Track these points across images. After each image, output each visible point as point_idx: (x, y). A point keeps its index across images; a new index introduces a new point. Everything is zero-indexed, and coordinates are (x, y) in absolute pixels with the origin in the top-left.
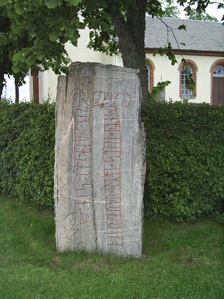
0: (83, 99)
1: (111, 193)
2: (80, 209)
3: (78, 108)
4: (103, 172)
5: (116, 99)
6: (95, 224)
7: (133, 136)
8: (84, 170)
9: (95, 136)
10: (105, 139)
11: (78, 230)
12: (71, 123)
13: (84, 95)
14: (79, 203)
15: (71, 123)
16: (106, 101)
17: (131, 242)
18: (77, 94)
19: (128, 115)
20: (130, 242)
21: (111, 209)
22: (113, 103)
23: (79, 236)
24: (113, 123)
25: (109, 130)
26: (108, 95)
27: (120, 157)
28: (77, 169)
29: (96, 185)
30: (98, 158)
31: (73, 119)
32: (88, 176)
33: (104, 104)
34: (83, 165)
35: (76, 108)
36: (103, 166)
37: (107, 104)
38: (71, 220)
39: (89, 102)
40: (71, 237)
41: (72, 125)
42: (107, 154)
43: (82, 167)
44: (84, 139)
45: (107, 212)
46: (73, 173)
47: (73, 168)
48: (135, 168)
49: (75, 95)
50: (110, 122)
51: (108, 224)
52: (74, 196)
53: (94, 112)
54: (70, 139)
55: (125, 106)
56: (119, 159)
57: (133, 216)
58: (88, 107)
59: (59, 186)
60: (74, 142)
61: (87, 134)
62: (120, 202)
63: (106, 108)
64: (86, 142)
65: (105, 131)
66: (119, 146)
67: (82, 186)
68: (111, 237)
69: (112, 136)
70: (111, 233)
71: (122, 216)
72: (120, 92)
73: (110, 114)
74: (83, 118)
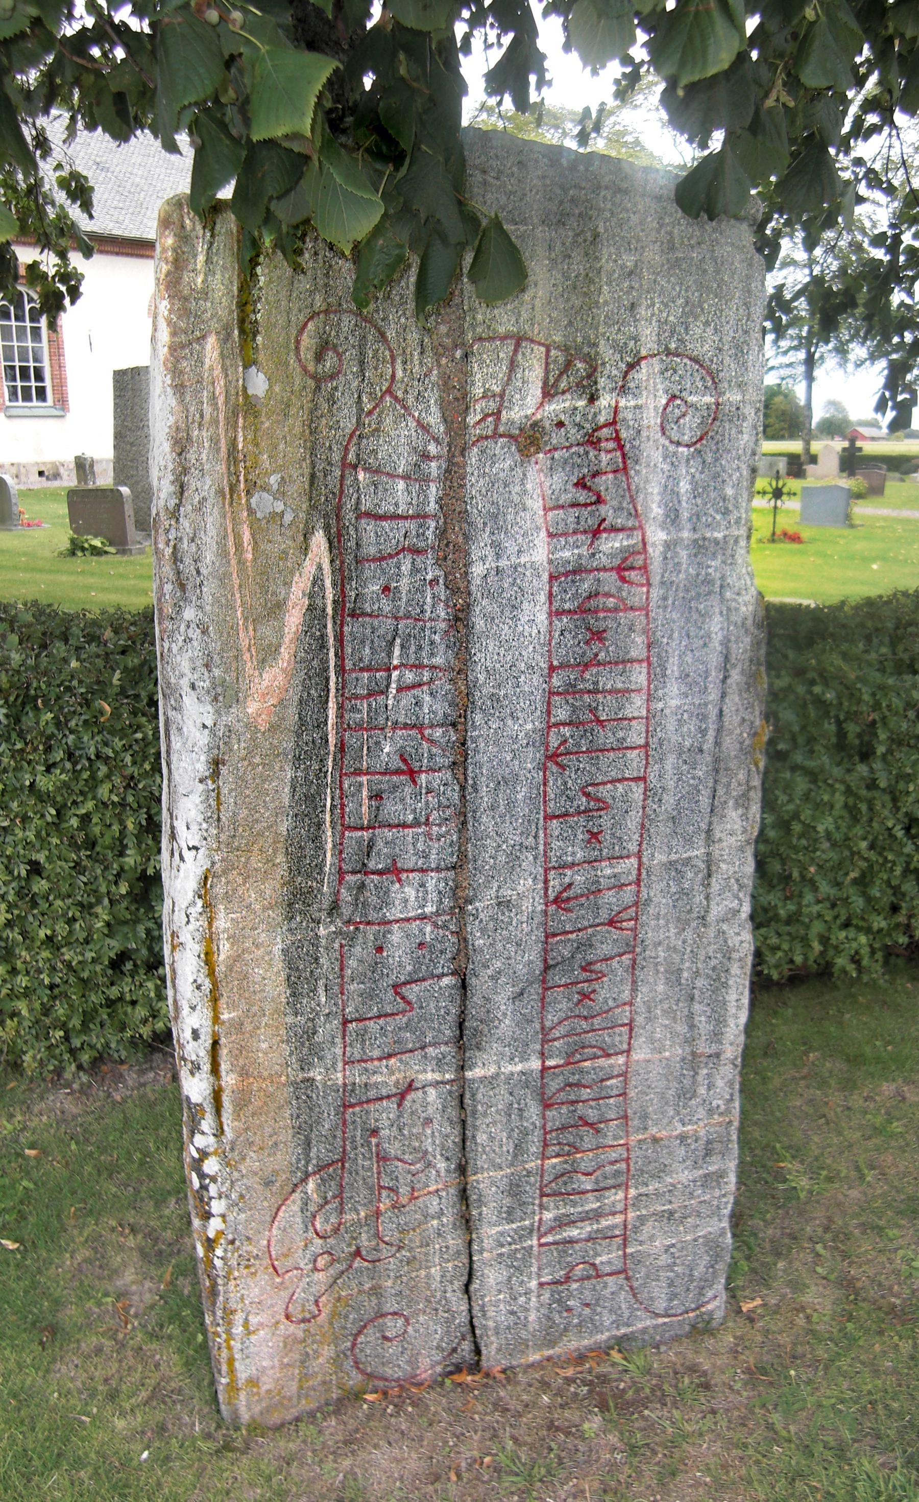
0: (389, 391)
1: (580, 1001)
2: (375, 1132)
3: (351, 457)
4: (540, 885)
5: (623, 390)
6: (464, 1195)
7: (726, 642)
8: (410, 892)
9: (486, 655)
10: (552, 669)
11: (358, 1253)
12: (309, 568)
13: (393, 357)
14: (368, 1101)
15: (309, 568)
16: (554, 407)
17: (679, 1246)
18: (335, 348)
19: (699, 501)
20: (673, 1245)
21: (572, 1097)
22: (602, 419)
23: (367, 1286)
24: (605, 561)
25: (582, 610)
26: (569, 364)
27: (643, 779)
28: (362, 887)
29: (489, 972)
30: (511, 804)
31: (319, 540)
32: (435, 925)
33: (547, 424)
34: (409, 860)
35: (336, 457)
36: (541, 848)
37: (560, 424)
38: (312, 1208)
39: (433, 409)
40: (316, 1302)
41: (317, 581)
42: (563, 767)
43: (394, 871)
44: (410, 677)
45: (544, 1118)
46: (330, 914)
47: (324, 879)
48: (723, 835)
49: (319, 357)
50: (584, 551)
51: (547, 1178)
52: (334, 1065)
53: (475, 484)
54: (306, 688)
55: (678, 444)
56: (641, 790)
57: (700, 1110)
58: (432, 449)
59: (225, 1016)
60: (332, 705)
61: (432, 643)
62: (625, 1047)
63: (557, 455)
64: (427, 698)
65: (550, 614)
66: (644, 713)
67: (391, 991)
68: (561, 1247)
69: (596, 646)
70: (562, 1222)
71: (635, 1122)
72: (649, 344)
73: (582, 496)
74: (395, 532)
